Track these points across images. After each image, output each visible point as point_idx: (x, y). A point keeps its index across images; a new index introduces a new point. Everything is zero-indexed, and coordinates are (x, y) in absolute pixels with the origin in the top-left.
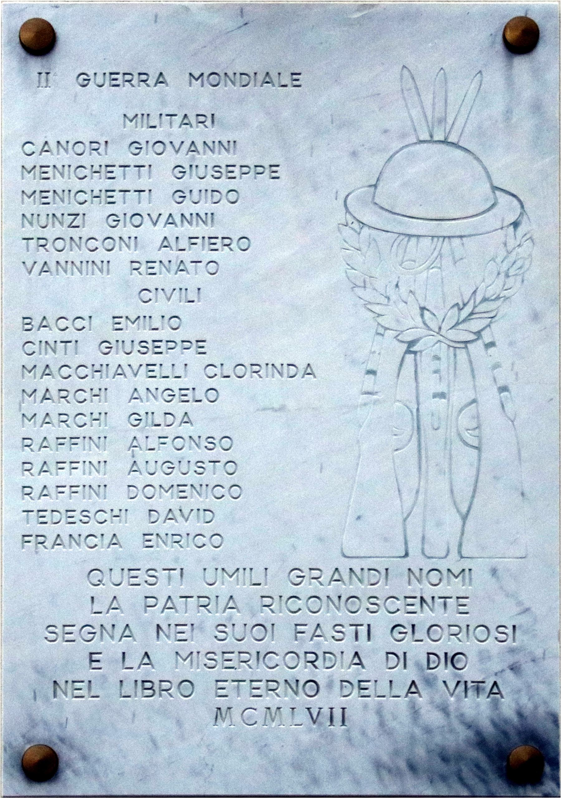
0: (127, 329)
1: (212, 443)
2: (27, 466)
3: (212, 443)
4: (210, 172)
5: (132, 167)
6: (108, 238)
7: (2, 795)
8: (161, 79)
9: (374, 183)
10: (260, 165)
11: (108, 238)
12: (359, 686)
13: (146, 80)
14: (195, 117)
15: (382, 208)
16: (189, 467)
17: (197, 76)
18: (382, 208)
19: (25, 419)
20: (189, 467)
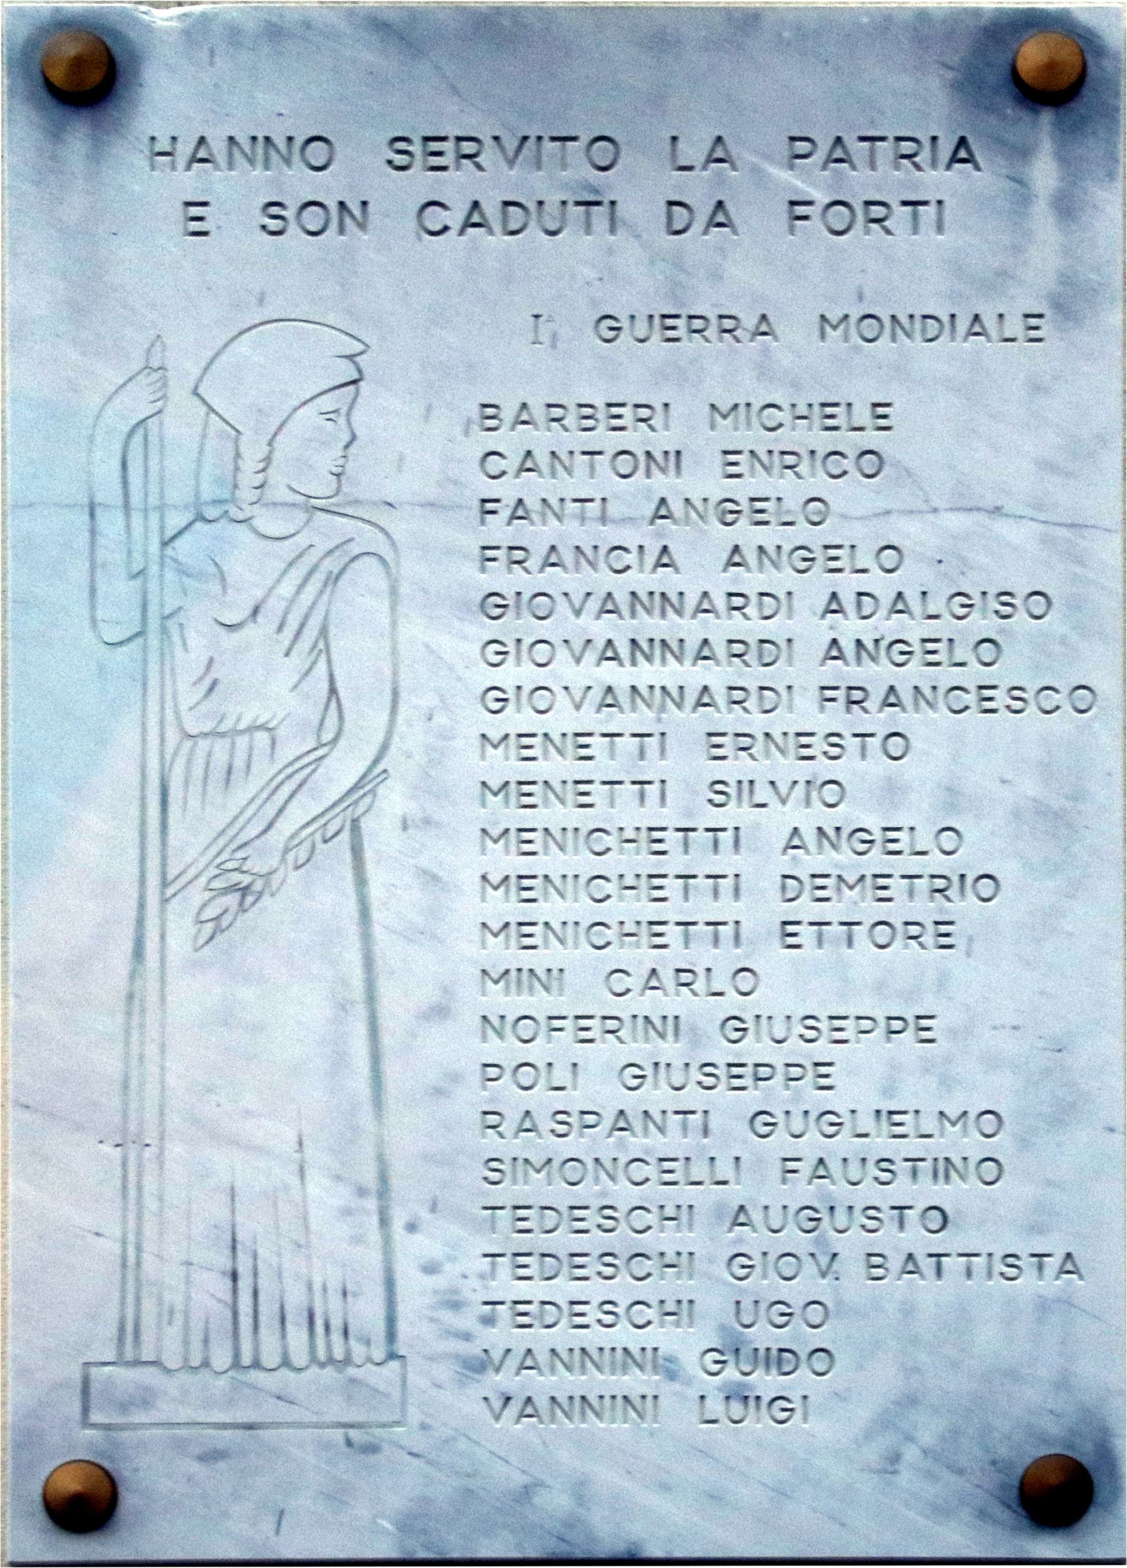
0: (575, 1088)
1: (813, 1028)
2: (492, 1119)
3: (813, 1028)
4: (696, 1075)
5: (671, 875)
6: (526, 1017)
7: (9, 1558)
8: (764, 327)
9: (198, 525)
10: (803, 135)
11: (526, 1017)
12: (917, 1024)
13: (649, 419)
14: (724, 597)
15: (217, 354)
16: (789, 1029)
17: (953, 1116)
18: (217, 354)
19: (843, 886)
20: (789, 1029)
